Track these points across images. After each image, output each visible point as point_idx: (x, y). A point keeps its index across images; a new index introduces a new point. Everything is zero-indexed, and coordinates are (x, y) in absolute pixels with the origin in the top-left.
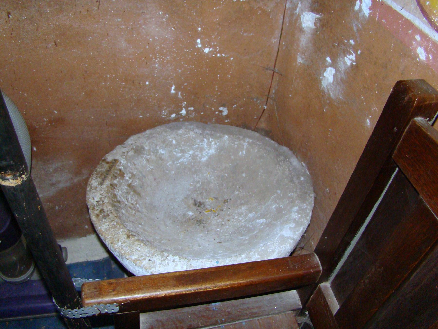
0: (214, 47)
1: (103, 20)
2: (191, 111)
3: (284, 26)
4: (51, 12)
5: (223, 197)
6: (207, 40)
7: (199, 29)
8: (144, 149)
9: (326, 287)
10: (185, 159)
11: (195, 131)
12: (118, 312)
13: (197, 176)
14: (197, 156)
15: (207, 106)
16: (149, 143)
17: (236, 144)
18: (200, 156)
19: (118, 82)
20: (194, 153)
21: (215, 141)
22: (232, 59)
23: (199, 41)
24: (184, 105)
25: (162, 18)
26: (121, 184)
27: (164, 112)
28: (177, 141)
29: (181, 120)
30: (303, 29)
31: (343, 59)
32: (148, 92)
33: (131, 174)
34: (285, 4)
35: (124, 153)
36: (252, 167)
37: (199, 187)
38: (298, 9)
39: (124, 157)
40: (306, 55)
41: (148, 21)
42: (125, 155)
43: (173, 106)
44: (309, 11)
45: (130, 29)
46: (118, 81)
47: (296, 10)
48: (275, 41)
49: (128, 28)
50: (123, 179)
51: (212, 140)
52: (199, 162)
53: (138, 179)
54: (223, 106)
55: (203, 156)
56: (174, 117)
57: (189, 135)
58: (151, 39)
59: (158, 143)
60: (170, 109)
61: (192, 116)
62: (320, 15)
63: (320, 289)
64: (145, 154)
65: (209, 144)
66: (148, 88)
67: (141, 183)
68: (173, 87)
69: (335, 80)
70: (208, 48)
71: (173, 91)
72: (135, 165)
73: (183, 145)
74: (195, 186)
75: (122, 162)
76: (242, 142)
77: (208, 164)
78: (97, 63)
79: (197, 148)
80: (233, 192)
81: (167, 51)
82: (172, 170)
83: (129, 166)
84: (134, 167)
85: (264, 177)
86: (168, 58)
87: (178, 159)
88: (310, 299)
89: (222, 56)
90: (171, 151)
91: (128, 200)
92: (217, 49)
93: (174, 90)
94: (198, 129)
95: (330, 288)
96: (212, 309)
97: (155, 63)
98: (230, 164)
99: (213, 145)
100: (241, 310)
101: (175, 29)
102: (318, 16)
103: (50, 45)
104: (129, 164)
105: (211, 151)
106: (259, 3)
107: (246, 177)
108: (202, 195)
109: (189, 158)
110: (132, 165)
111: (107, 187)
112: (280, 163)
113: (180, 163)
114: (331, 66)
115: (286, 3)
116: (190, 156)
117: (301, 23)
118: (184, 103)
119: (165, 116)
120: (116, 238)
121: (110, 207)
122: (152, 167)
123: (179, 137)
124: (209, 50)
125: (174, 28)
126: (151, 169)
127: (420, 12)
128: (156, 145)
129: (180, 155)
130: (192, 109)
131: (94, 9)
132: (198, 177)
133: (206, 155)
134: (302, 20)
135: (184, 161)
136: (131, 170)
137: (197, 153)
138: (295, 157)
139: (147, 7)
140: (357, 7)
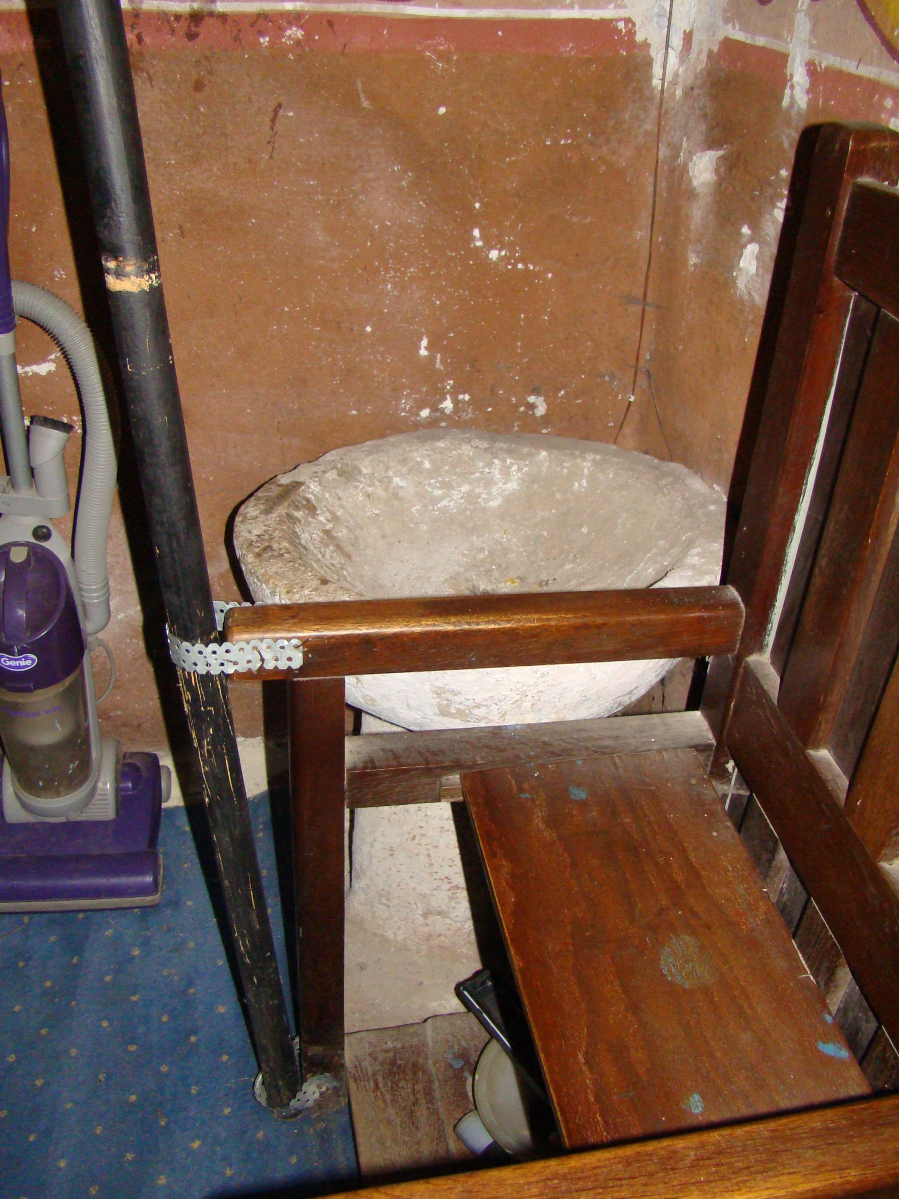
0: (511, 246)
1: (279, 181)
2: (464, 402)
3: (657, 199)
4: (178, 163)
5: (539, 576)
6: (494, 232)
7: (477, 205)
8: (360, 472)
9: (760, 664)
10: (453, 501)
11: (473, 442)
12: (302, 671)
13: (478, 537)
14: (479, 496)
15: (501, 392)
16: (372, 461)
17: (566, 468)
18: (485, 496)
19: (305, 325)
20: (472, 490)
21: (518, 465)
22: (550, 275)
23: (476, 233)
24: (448, 387)
25: (400, 180)
26: (309, 524)
27: (405, 403)
28: (432, 462)
29: (443, 424)
30: (695, 189)
31: (771, 214)
32: (369, 350)
33: (331, 514)
34: (656, 151)
35: (316, 472)
36: (602, 512)
37: (482, 561)
38: (682, 154)
39: (317, 479)
40: (704, 242)
41: (370, 186)
42: (318, 477)
43: (424, 389)
44: (703, 150)
45: (334, 202)
46: (305, 322)
47: (679, 156)
48: (640, 234)
49: (329, 200)
50: (313, 517)
51: (511, 463)
52: (484, 509)
53: (346, 527)
54: (536, 391)
55: (491, 497)
56: (427, 417)
57: (461, 452)
58: (376, 227)
59: (392, 464)
60: (417, 396)
61: (467, 415)
62: (724, 149)
63: (747, 669)
64: (362, 482)
65: (506, 472)
66: (370, 342)
67: (352, 536)
68: (424, 343)
69: (761, 265)
70: (496, 249)
71: (423, 352)
72: (339, 499)
73: (447, 472)
74: (475, 557)
75: (312, 487)
76: (579, 461)
77: (503, 513)
78: (264, 279)
79: (478, 480)
80: (562, 566)
81: (410, 253)
82: (423, 523)
83: (327, 499)
84: (337, 501)
85: (629, 526)
86: (412, 269)
87: (435, 501)
88: (731, 712)
89: (527, 267)
90: (420, 483)
91: (323, 556)
92: (516, 252)
93: (426, 348)
94: (480, 440)
95: (771, 666)
96: (506, 736)
97: (385, 282)
98: (554, 511)
99: (514, 473)
100: (573, 741)
101: (426, 204)
102: (721, 153)
103: (171, 235)
104: (327, 495)
105: (509, 486)
106: (601, 147)
107: (589, 532)
108: (491, 576)
109: (461, 501)
110: (334, 498)
111: (280, 516)
112: (665, 490)
113: (439, 509)
114: (752, 240)
115: (658, 148)
116: (462, 498)
117: (690, 180)
118: (449, 382)
119: (406, 412)
120: (297, 584)
121: (285, 544)
122: (377, 512)
123: (438, 456)
124: (500, 253)
125: (424, 201)
126: (376, 515)
127: (888, 55)
128: (387, 469)
129: (438, 492)
130: (467, 397)
131: (262, 158)
132: (480, 540)
133: (499, 494)
134: (691, 174)
135: (449, 506)
136: (332, 506)
137: (477, 491)
138: (700, 480)
139: (369, 156)
140: (785, 102)
